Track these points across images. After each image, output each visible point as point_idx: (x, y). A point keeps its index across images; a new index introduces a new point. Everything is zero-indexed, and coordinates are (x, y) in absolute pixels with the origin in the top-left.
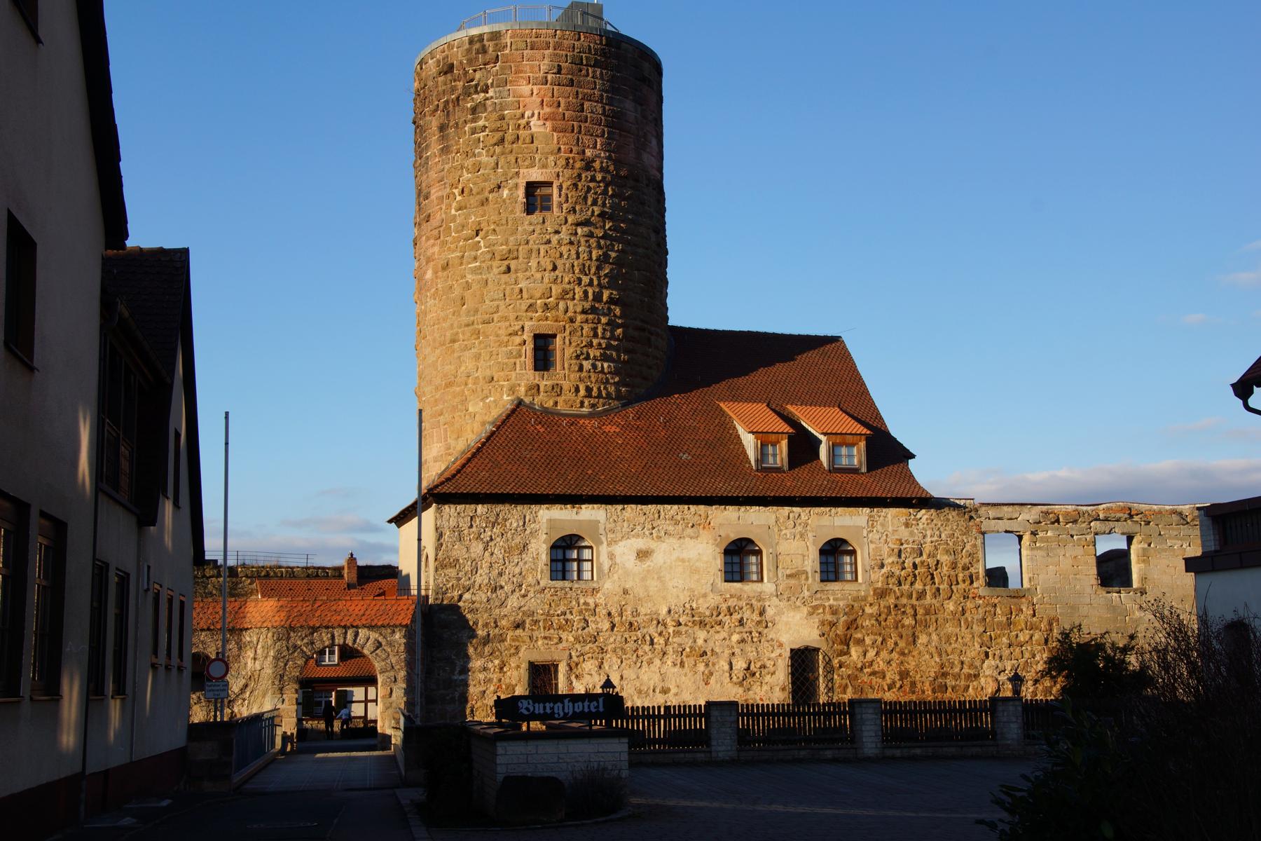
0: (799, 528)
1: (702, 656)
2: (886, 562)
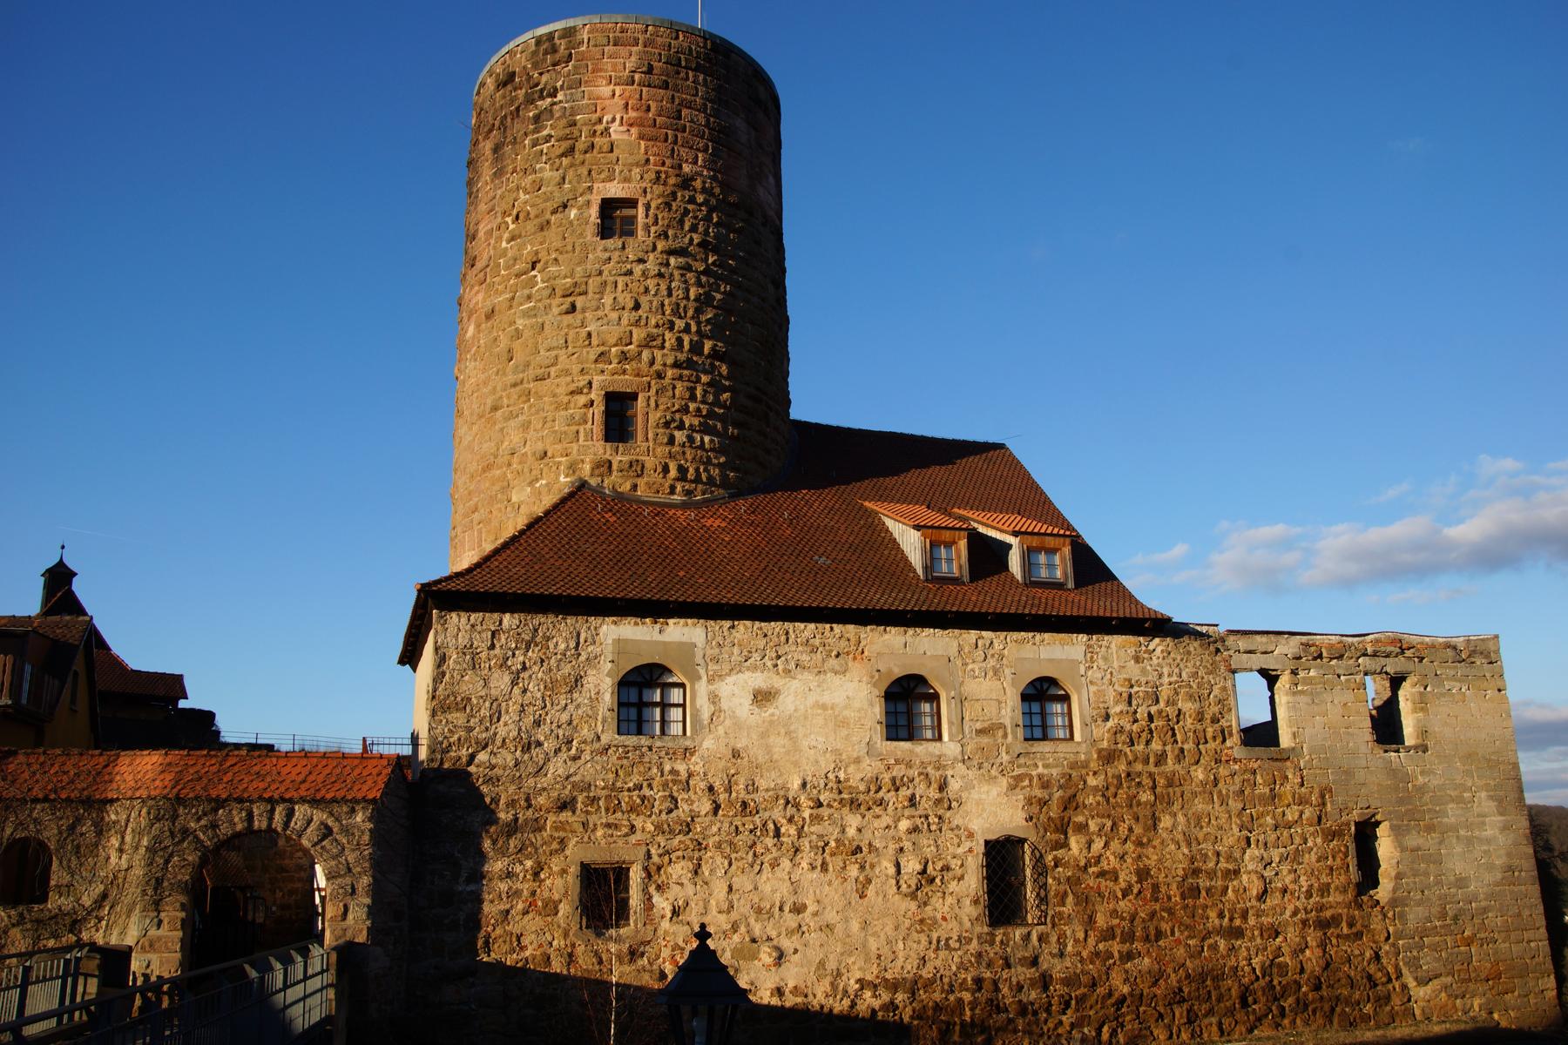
0: (991, 662)
1: (854, 853)
2: (1112, 712)
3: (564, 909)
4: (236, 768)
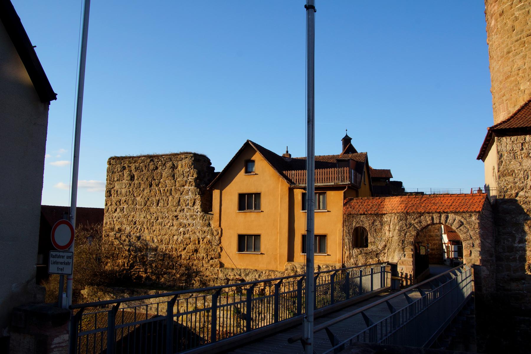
4: (426, 201)
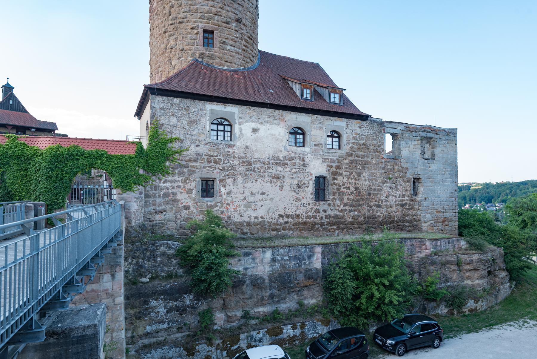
3: (194, 192)
